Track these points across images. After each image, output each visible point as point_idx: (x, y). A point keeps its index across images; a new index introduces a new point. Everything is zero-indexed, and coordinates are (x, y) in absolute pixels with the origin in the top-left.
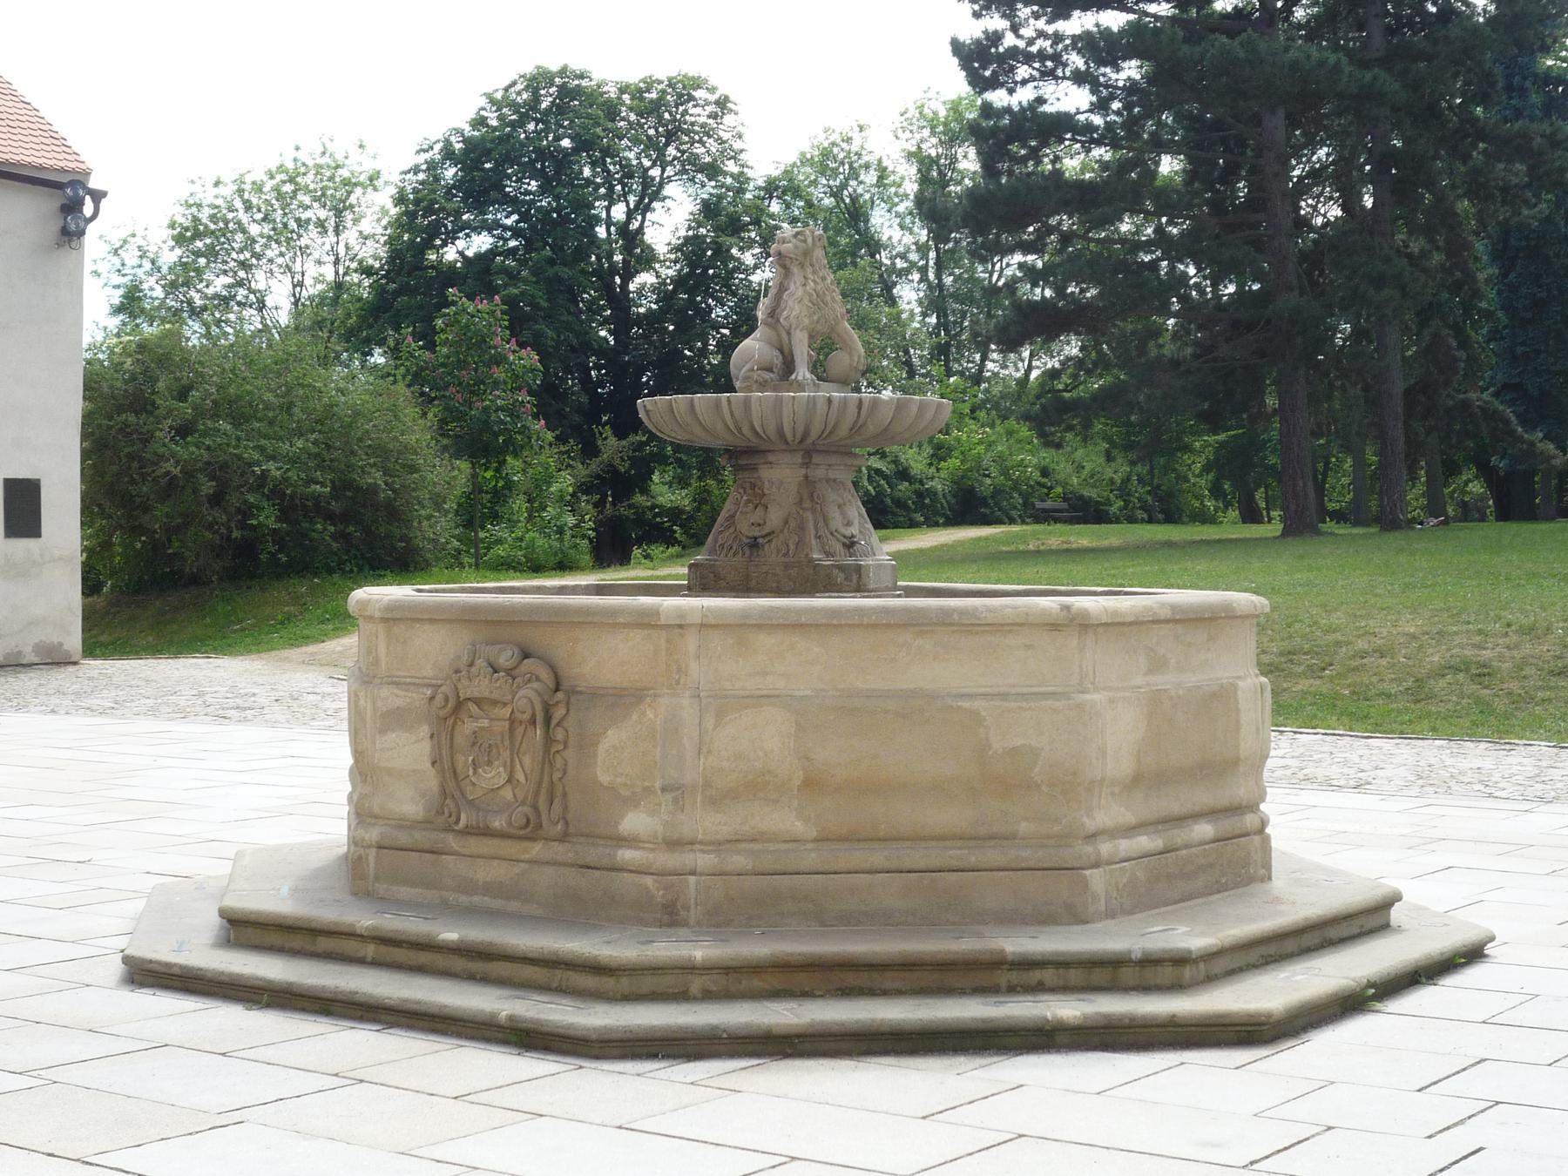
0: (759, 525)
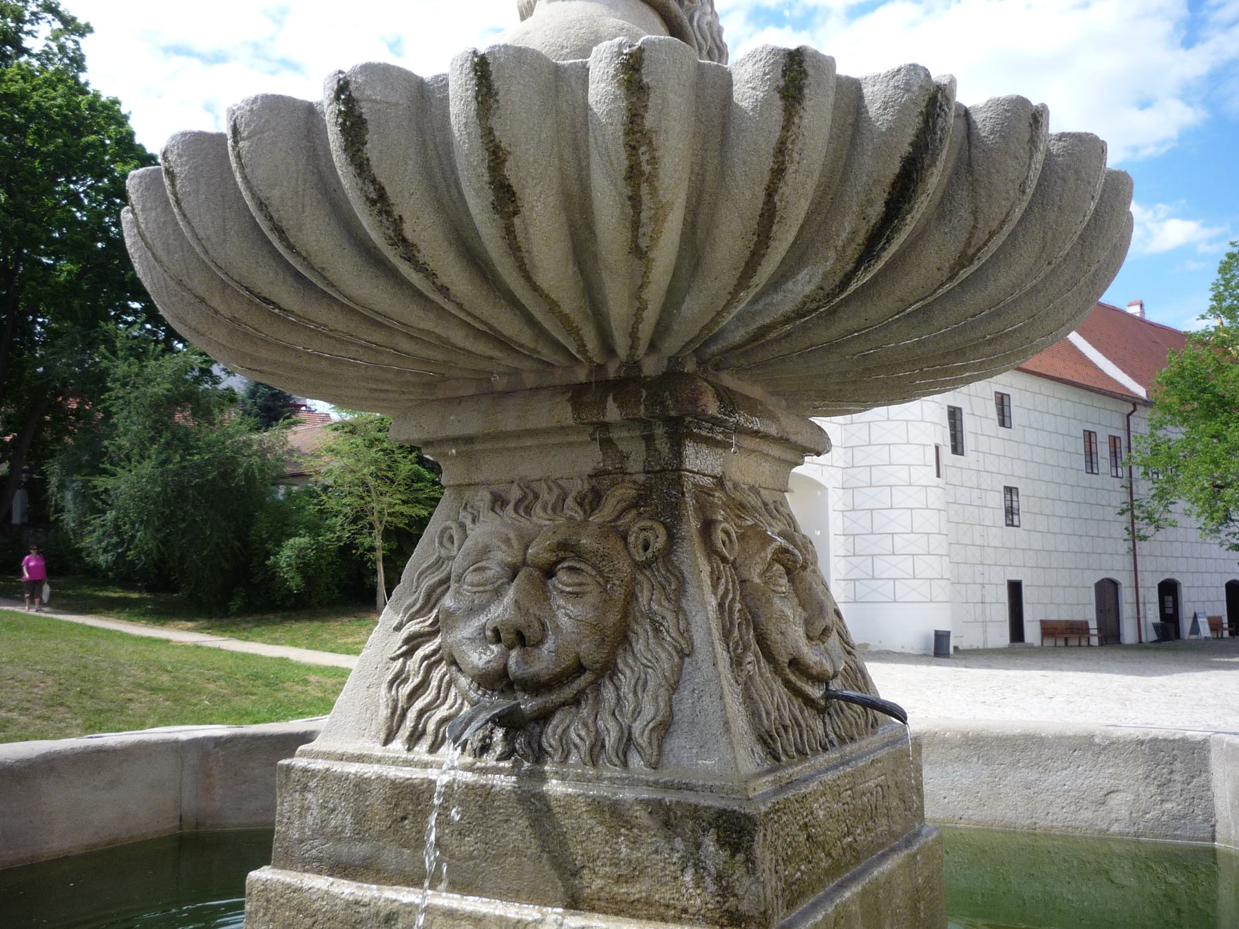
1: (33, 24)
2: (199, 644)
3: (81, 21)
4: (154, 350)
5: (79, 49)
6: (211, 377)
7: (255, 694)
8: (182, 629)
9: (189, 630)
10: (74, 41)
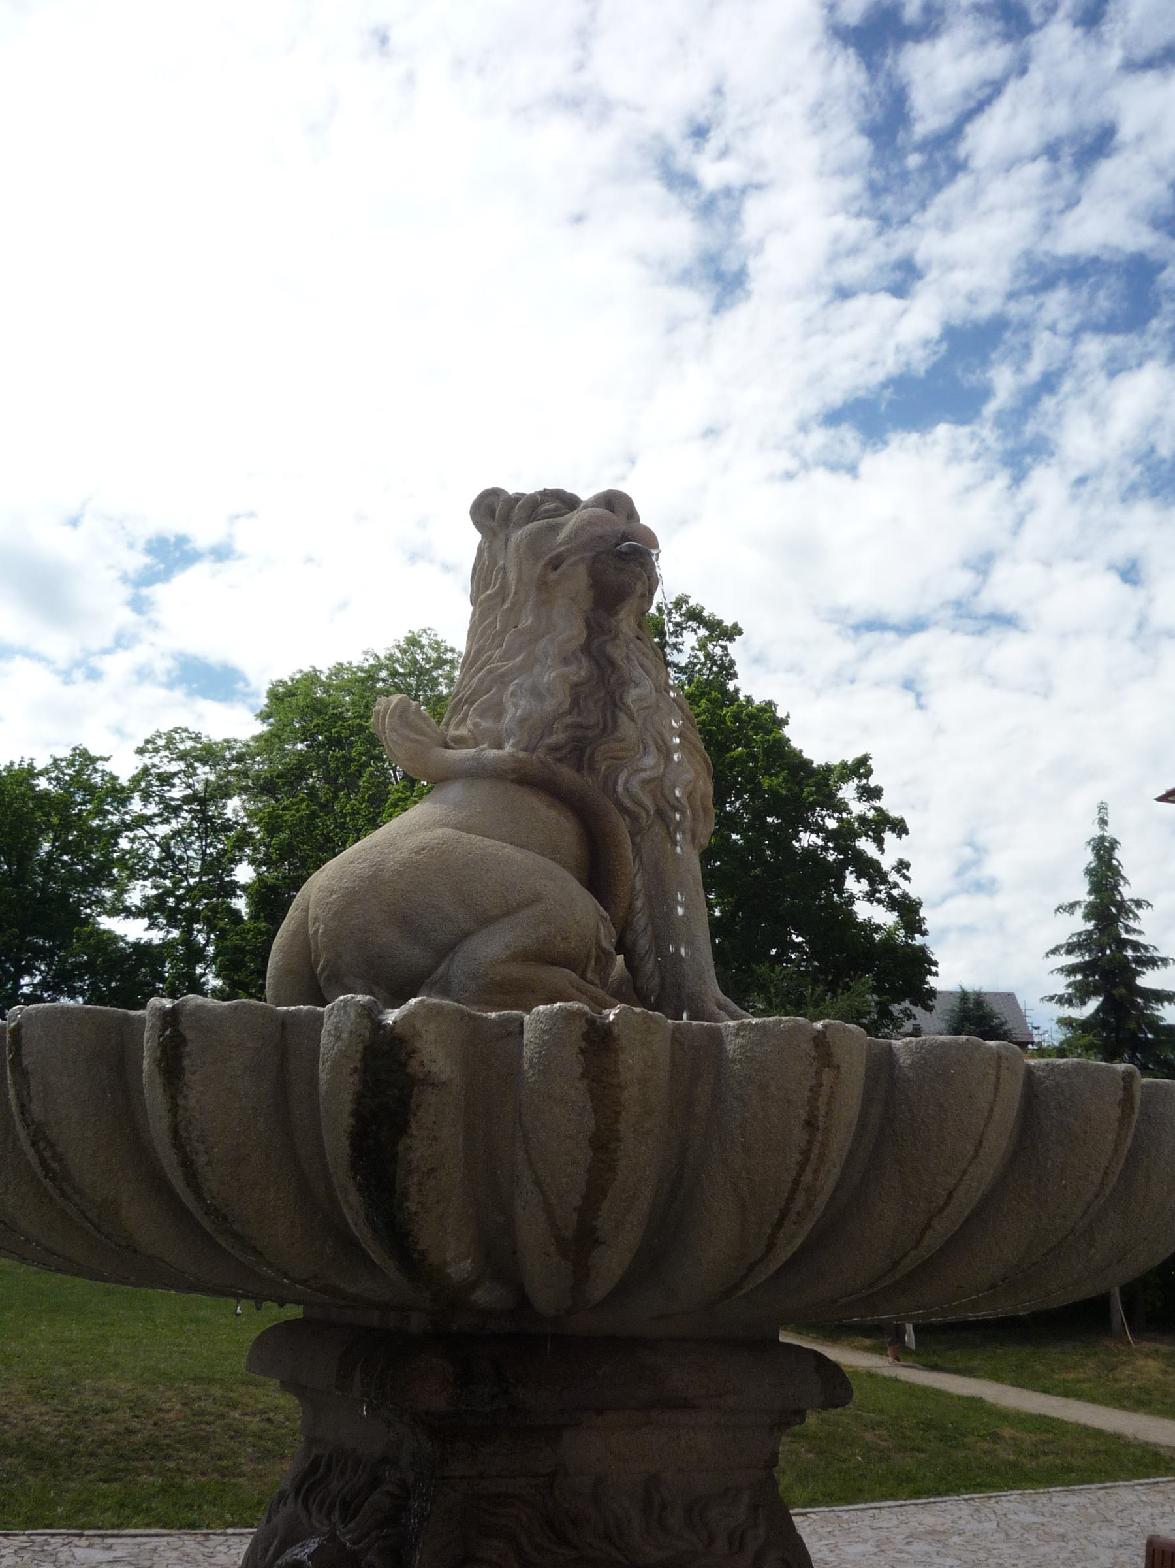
1: (677, 637)
2: (873, 1370)
3: (728, 623)
4: (812, 994)
5: (727, 655)
6: (892, 1020)
7: (923, 1451)
8: (857, 1348)
9: (867, 1349)
10: (722, 647)
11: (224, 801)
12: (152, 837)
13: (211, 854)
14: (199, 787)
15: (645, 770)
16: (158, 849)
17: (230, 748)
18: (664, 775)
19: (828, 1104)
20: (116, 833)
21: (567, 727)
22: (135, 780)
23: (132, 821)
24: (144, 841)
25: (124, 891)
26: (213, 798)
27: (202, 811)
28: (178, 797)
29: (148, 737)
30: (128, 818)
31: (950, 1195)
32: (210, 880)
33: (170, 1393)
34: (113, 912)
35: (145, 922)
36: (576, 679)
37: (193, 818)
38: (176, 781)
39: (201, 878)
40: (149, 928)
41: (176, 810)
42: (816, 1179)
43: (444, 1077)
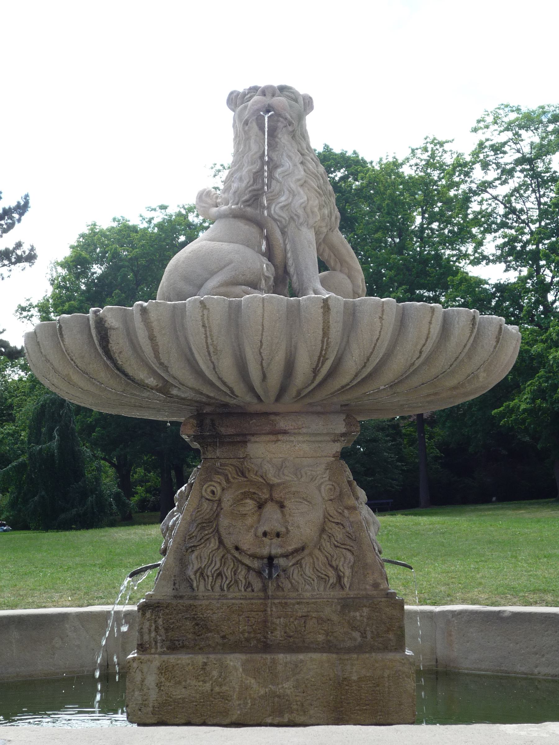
0: (278, 535)
11: (549, 157)
12: (495, 198)
13: (545, 203)
14: (527, 150)
15: (281, 202)
16: (502, 206)
17: (544, 113)
18: (291, 202)
19: (208, 319)
20: (466, 199)
21: (250, 191)
22: (475, 154)
23: (477, 188)
24: (490, 202)
25: (480, 244)
26: (538, 156)
27: (532, 169)
28: (510, 162)
29: (479, 118)
30: (474, 187)
31: (261, 342)
32: (547, 224)
33: (515, 600)
34: (476, 262)
35: (503, 266)
36: (254, 170)
37: (525, 176)
38: (506, 148)
39: (540, 224)
40: (506, 270)
41: (510, 173)
42: (213, 341)
43: (116, 327)
